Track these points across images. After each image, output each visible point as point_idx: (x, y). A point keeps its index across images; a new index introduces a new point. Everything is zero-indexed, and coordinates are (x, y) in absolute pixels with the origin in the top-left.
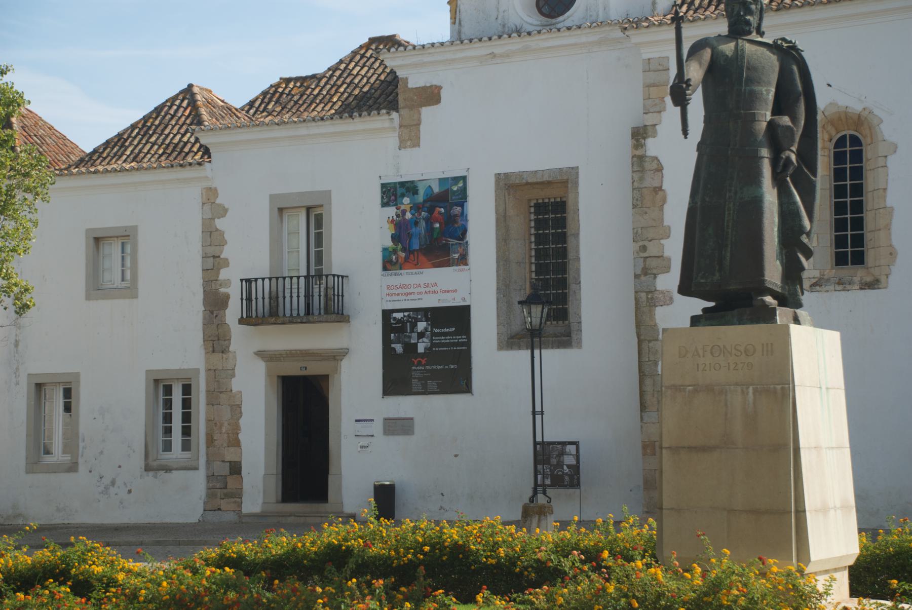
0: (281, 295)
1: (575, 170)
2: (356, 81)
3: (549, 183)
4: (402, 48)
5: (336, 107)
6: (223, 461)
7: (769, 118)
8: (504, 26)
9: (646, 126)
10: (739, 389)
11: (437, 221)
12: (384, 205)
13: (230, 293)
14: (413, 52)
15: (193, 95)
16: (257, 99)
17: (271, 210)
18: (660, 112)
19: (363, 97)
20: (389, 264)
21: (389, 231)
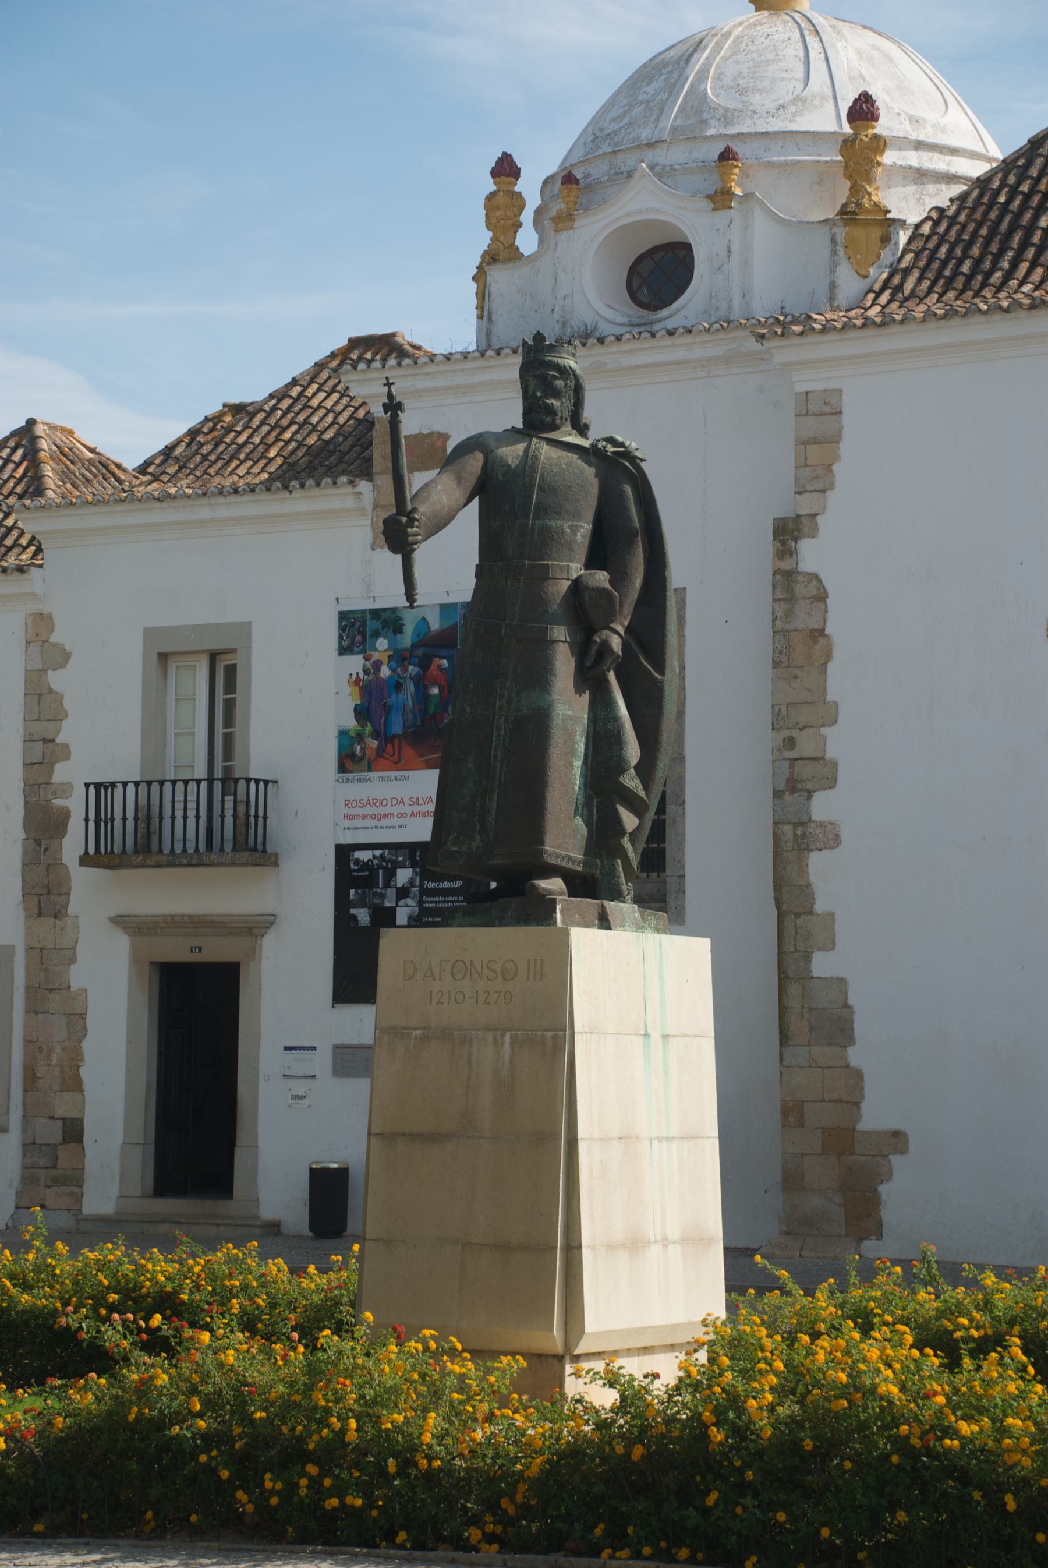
0: (155, 810)
2: (314, 420)
4: (406, 361)
5: (272, 468)
6: (52, 1118)
8: (564, 324)
9: (798, 516)
10: (490, 1036)
11: (435, 683)
12: (344, 650)
13: (71, 808)
14: (431, 368)
15: (34, 439)
16: (178, 442)
18: (824, 491)
19: (321, 450)
20: (349, 760)
21: (350, 699)
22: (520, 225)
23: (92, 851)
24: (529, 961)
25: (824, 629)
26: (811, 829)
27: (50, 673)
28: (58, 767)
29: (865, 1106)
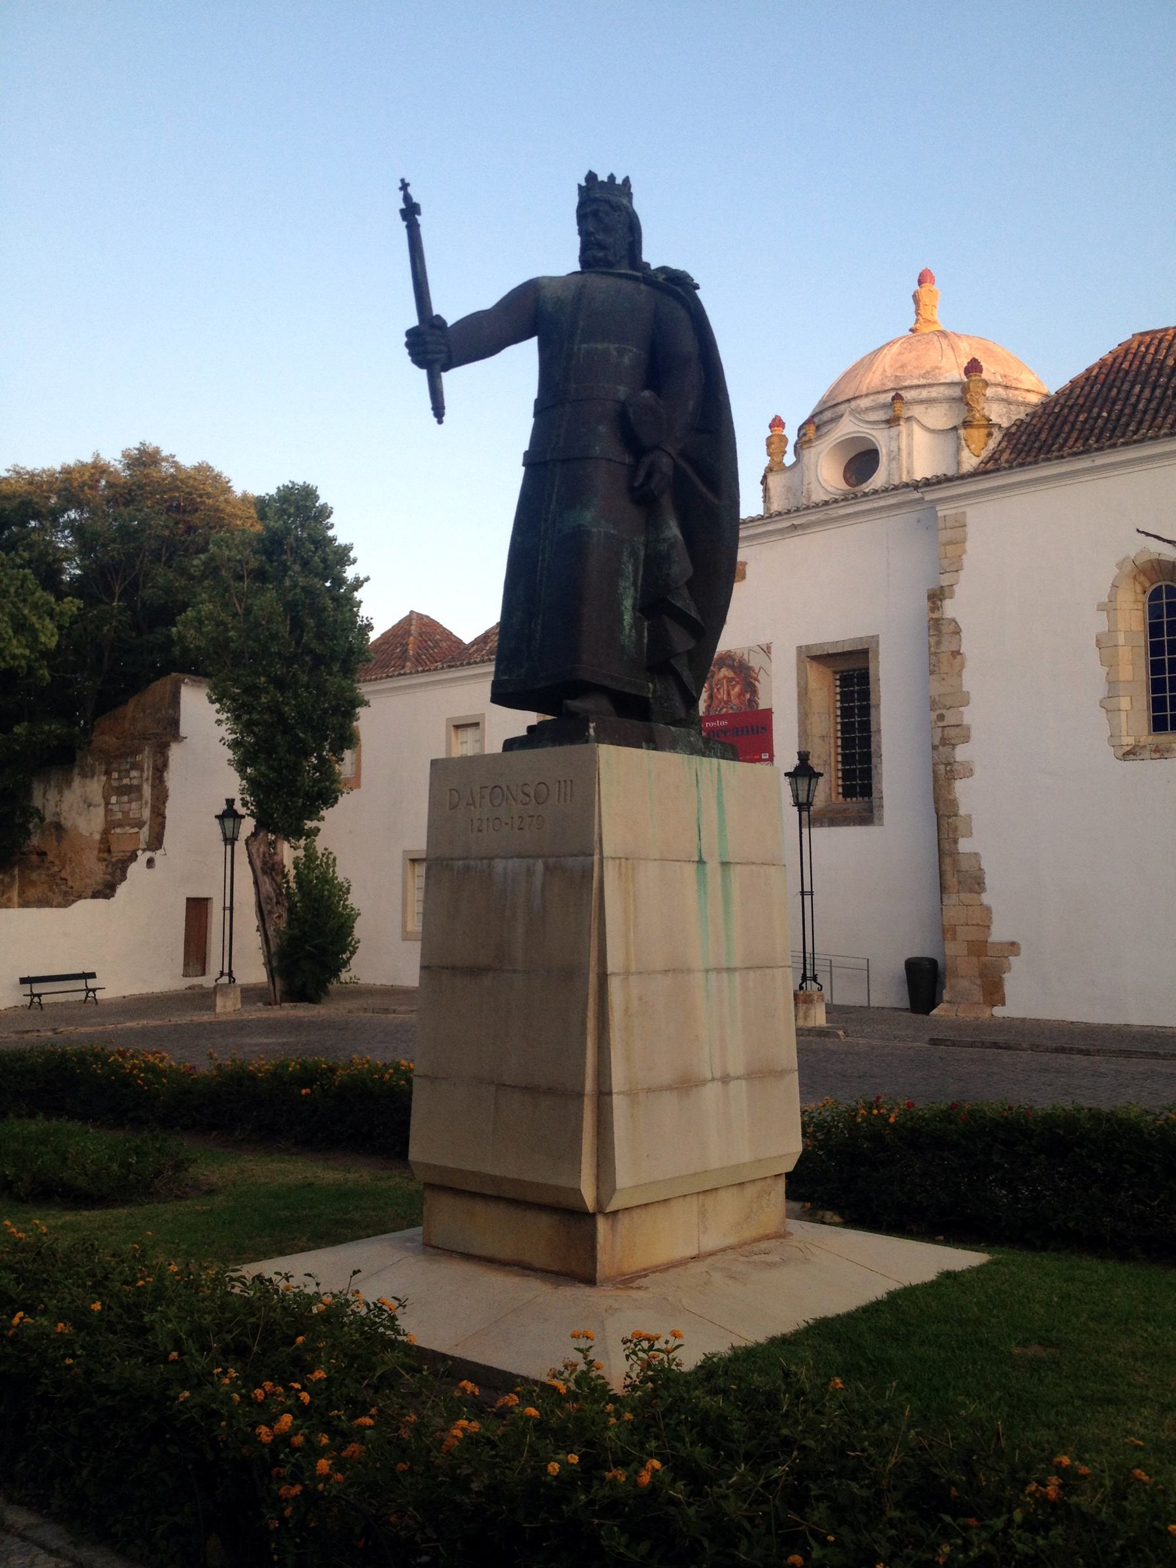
1: (875, 639)
3: (850, 653)
22: (785, 452)
26: (956, 766)
29: (993, 929)
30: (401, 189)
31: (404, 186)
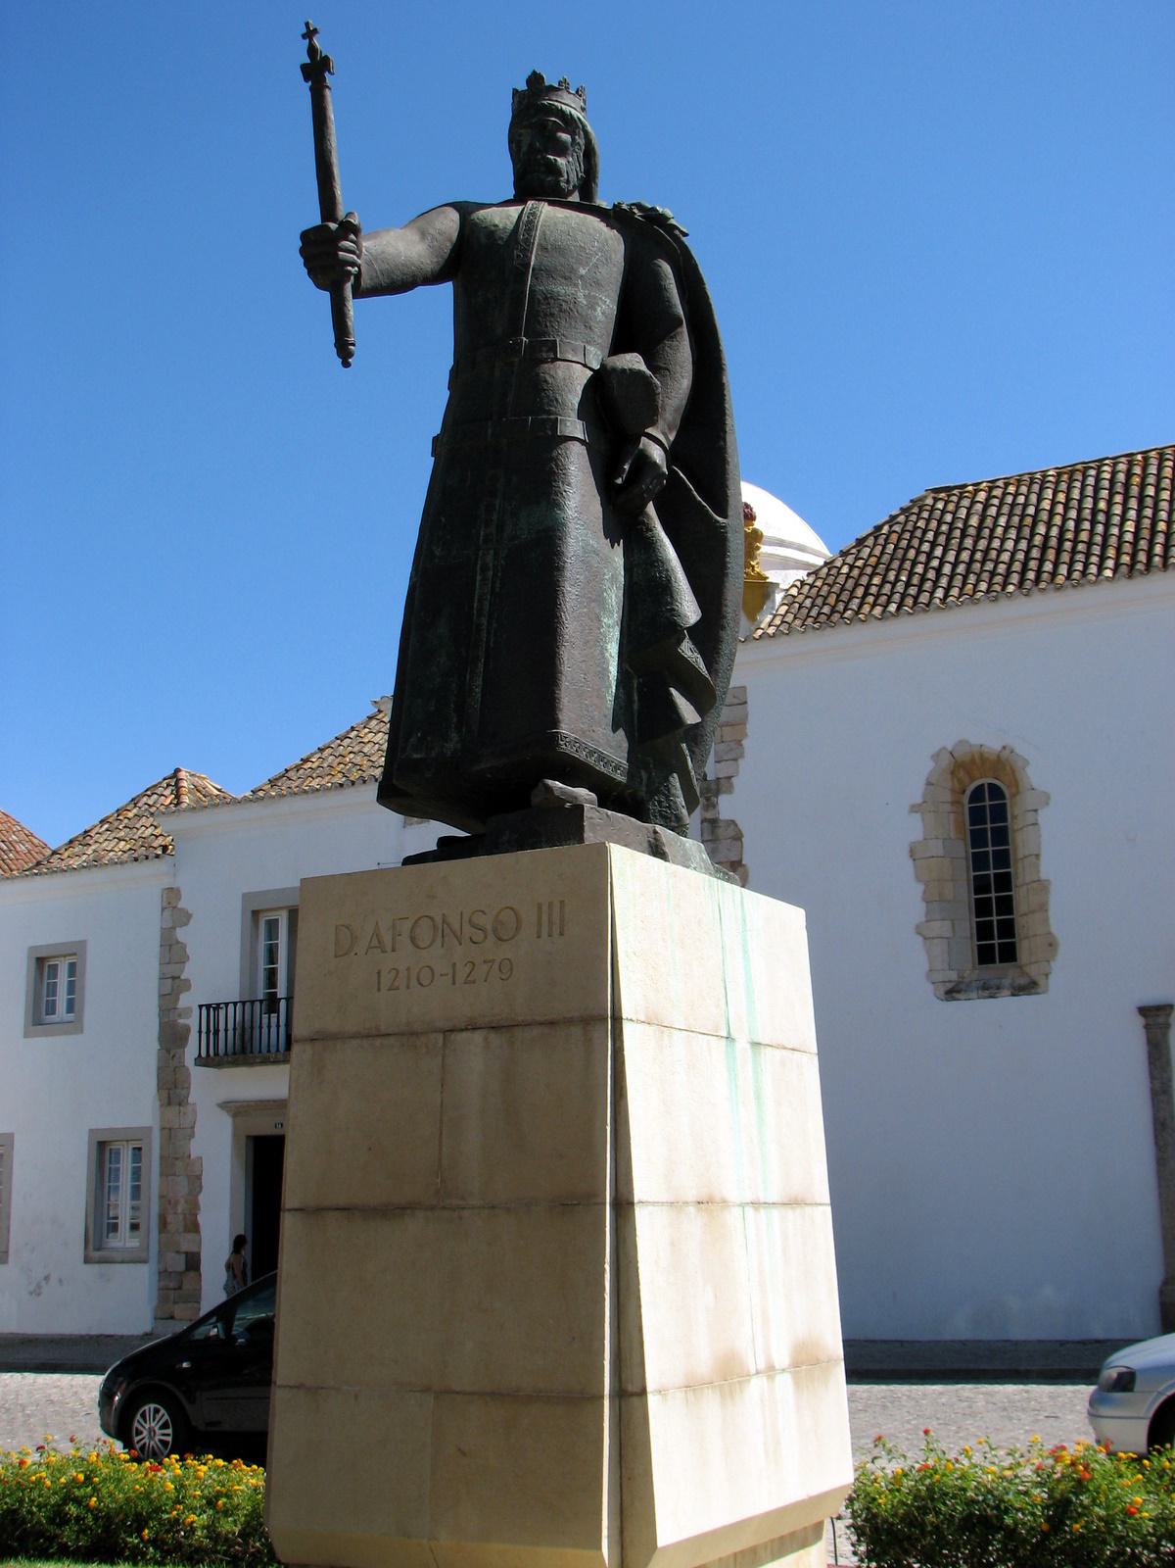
7: (596, 358)
9: (718, 779)
13: (191, 1025)
17: (243, 913)
18: (735, 760)
23: (204, 1054)
24: (540, 907)
25: (741, 861)
27: (178, 929)
28: (182, 996)
30: (304, 36)
31: (310, 34)
